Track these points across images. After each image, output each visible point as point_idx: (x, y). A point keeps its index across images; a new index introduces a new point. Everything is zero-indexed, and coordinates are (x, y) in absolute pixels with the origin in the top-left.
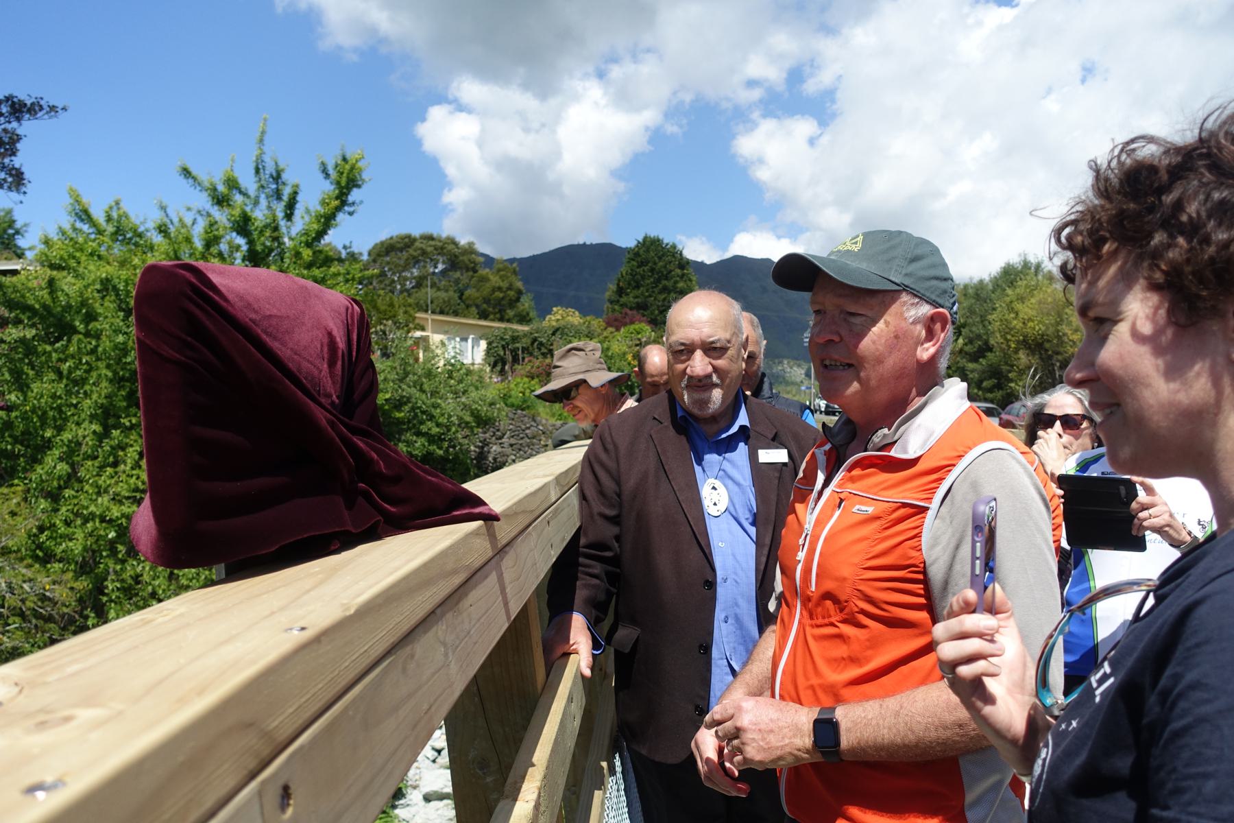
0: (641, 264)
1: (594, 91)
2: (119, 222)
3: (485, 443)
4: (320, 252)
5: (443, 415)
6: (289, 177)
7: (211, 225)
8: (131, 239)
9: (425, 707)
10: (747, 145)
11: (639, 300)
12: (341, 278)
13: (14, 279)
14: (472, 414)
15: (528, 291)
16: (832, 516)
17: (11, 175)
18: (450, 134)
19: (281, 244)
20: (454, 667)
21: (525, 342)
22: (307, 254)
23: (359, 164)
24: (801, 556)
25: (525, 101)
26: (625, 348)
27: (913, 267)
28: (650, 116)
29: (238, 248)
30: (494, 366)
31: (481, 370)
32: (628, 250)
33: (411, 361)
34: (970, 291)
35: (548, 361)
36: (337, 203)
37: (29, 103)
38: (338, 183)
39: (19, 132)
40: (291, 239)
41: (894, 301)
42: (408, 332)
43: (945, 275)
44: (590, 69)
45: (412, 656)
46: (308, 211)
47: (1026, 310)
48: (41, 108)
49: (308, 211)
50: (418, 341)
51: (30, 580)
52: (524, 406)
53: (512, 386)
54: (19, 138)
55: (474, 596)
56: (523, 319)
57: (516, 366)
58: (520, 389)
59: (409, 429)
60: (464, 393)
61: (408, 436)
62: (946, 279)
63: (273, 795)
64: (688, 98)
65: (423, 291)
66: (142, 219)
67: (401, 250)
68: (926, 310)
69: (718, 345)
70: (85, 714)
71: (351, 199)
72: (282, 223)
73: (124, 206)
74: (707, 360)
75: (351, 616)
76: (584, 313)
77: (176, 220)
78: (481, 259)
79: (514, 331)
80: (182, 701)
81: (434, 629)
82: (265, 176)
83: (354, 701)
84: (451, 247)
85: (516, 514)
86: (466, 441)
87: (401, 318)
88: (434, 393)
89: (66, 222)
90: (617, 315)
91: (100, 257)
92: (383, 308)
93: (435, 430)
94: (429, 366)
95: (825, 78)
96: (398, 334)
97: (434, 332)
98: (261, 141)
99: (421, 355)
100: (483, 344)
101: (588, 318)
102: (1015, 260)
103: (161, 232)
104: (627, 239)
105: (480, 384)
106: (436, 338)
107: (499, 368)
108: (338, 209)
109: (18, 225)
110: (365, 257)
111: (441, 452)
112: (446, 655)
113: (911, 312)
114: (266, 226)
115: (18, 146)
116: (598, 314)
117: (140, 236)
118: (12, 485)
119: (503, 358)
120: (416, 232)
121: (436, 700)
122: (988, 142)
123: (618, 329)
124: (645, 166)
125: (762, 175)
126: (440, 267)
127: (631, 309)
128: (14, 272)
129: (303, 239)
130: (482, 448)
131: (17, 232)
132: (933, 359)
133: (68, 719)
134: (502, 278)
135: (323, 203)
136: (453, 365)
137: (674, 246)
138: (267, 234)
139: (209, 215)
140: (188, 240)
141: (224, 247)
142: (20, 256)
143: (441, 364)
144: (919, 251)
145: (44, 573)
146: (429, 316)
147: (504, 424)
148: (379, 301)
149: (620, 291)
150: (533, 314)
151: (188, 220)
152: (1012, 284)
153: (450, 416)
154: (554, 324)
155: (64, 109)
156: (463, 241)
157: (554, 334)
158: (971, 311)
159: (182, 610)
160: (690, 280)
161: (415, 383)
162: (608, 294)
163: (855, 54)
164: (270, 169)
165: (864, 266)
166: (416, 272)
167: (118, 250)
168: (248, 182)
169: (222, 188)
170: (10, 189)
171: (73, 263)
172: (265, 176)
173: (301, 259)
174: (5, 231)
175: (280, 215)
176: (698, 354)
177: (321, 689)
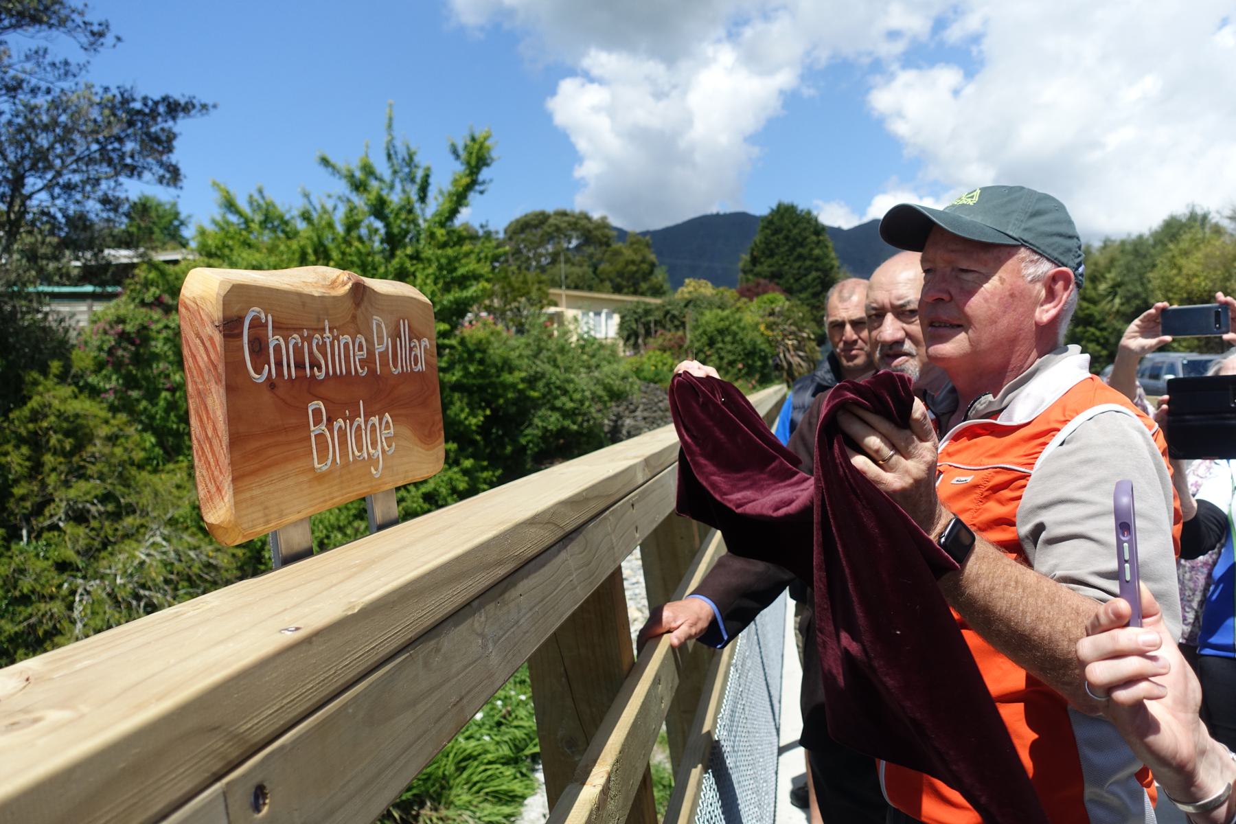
1: (726, 56)
3: (619, 417)
4: (454, 231)
6: (422, 160)
7: (351, 210)
9: (454, 699)
10: (883, 99)
11: (774, 269)
15: (661, 264)
17: (169, 171)
18: (578, 106)
20: (494, 659)
21: (658, 315)
22: (440, 233)
25: (655, 68)
26: (757, 319)
27: (1032, 223)
28: (785, 79)
29: (376, 230)
30: (627, 339)
31: (613, 345)
32: (762, 219)
35: (680, 333)
37: (182, 102)
38: (468, 163)
39: (176, 130)
40: (425, 220)
41: (1010, 256)
42: (542, 308)
43: (1071, 233)
44: (721, 32)
45: (438, 650)
46: (441, 193)
48: (194, 106)
49: (441, 193)
50: (552, 318)
54: (175, 136)
55: (524, 585)
56: (657, 291)
57: (651, 340)
58: (653, 362)
59: (544, 404)
62: (1071, 237)
63: (243, 797)
64: (823, 56)
65: (558, 266)
66: (287, 207)
67: (536, 227)
68: (1046, 268)
69: (909, 308)
70: (54, 716)
71: (481, 177)
72: (417, 206)
73: (270, 195)
74: (899, 324)
75: (353, 615)
76: (716, 282)
77: (318, 207)
78: (615, 233)
79: (646, 304)
81: (470, 621)
83: (355, 699)
84: (584, 222)
86: (600, 415)
87: (534, 295)
90: (751, 284)
92: (517, 285)
93: (570, 405)
95: (972, 23)
96: (532, 310)
97: (569, 307)
98: (390, 126)
100: (616, 319)
101: (721, 289)
102: (1179, 209)
104: (761, 208)
105: (613, 357)
106: (570, 313)
107: (632, 341)
108: (469, 187)
109: (182, 216)
110: (501, 236)
111: (575, 427)
112: (485, 646)
113: (1031, 269)
114: (401, 209)
115: (175, 143)
116: (731, 285)
117: (286, 223)
118: (177, 462)
119: (633, 333)
120: (550, 209)
121: (469, 692)
122: (1150, 84)
123: (751, 300)
125: (901, 128)
126: (574, 243)
127: (765, 278)
129: (437, 219)
130: (616, 421)
131: (182, 223)
132: (1055, 321)
133: (36, 721)
134: (636, 251)
136: (585, 340)
137: (809, 213)
139: (349, 200)
140: (330, 225)
141: (363, 231)
143: (574, 339)
144: (1042, 206)
146: (563, 292)
147: (636, 397)
149: (754, 261)
150: (666, 286)
151: (329, 206)
153: (583, 391)
154: (687, 296)
155: (215, 106)
156: (596, 215)
157: (686, 306)
158: (1129, 269)
159: (216, 603)
160: (827, 247)
161: (549, 358)
162: (741, 265)
164: (402, 152)
165: (979, 219)
166: (550, 248)
167: (267, 237)
168: (382, 168)
169: (359, 175)
170: (168, 184)
171: (227, 251)
174: (171, 222)
175: (414, 197)
176: (889, 318)
177: (311, 689)
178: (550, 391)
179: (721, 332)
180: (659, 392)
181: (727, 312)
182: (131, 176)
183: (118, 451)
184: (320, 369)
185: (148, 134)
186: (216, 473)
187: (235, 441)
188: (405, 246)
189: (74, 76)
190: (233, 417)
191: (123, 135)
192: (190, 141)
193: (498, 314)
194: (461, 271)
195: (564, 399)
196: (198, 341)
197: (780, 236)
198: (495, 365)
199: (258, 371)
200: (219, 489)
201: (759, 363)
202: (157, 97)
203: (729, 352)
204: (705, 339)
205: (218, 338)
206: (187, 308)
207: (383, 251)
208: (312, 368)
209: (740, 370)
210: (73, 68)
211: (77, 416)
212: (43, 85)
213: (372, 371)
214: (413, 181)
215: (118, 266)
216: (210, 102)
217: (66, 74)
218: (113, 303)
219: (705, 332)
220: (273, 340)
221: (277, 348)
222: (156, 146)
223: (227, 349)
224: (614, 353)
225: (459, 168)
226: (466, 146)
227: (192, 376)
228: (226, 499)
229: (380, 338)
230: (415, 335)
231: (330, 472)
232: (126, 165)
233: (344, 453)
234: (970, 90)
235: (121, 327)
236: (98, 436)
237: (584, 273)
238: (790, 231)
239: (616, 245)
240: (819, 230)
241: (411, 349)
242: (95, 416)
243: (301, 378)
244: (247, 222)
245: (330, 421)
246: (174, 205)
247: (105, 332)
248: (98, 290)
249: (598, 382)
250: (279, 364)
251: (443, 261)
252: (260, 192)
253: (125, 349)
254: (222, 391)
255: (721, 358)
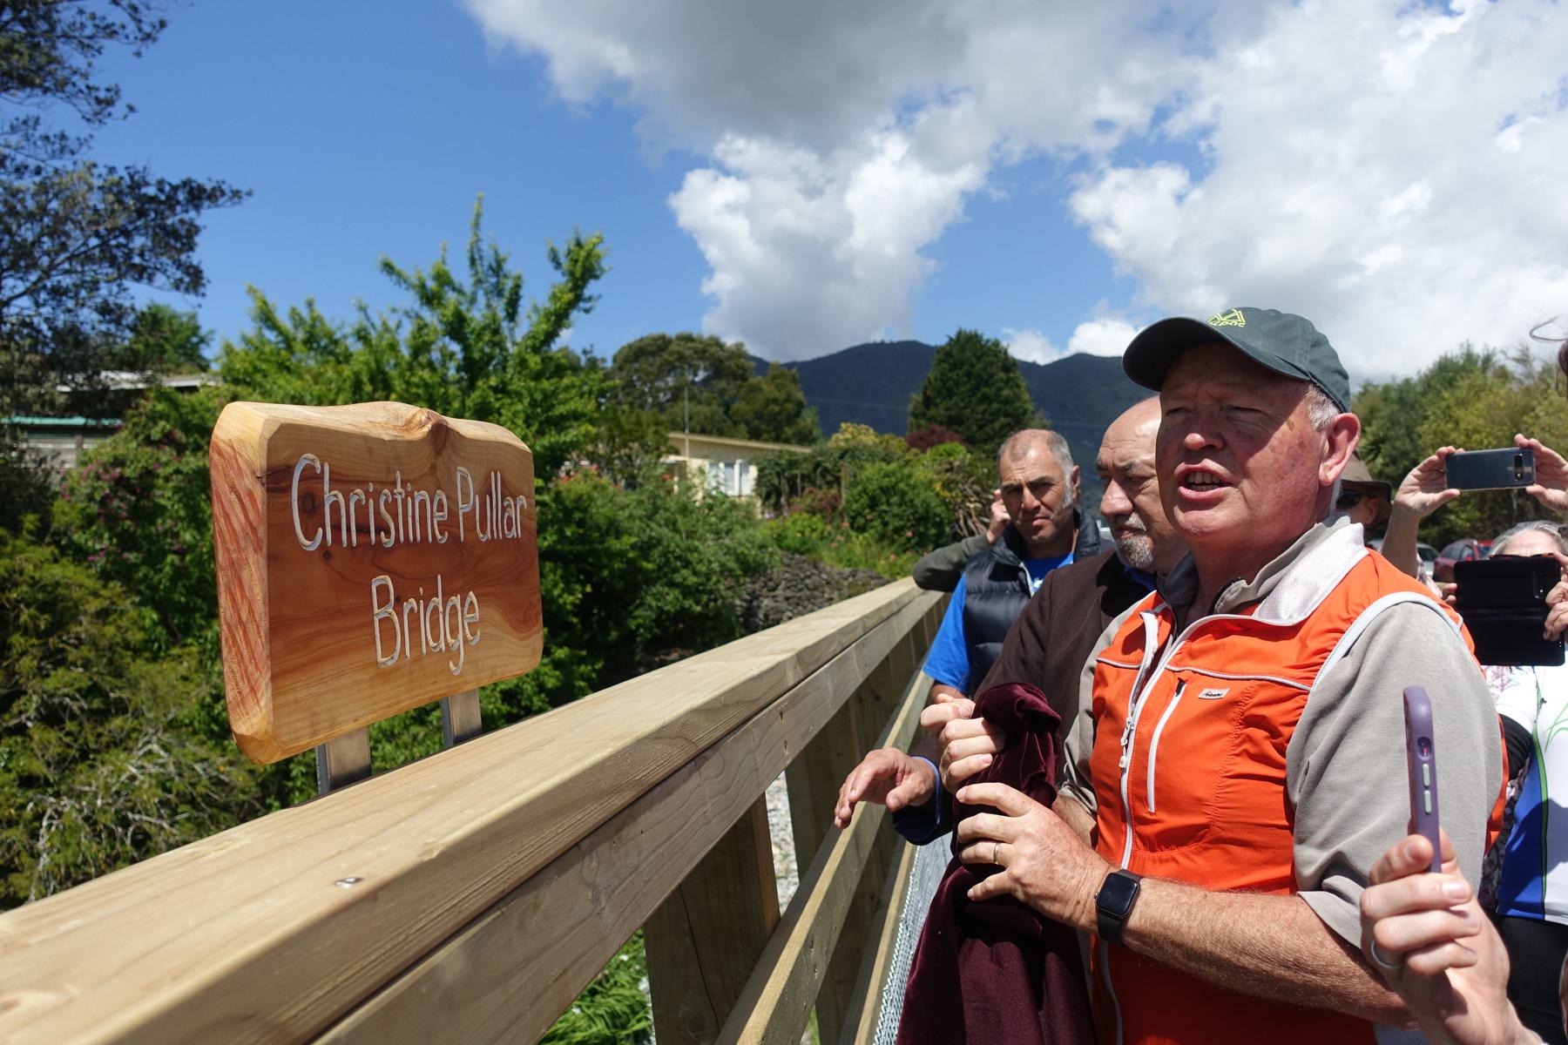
0: (954, 367)
1: (896, 147)
2: (313, 326)
3: (754, 596)
4: (551, 358)
5: (701, 561)
7: (420, 329)
8: (325, 347)
9: (557, 971)
10: (1088, 204)
12: (574, 391)
13: (193, 398)
14: (738, 560)
16: (1167, 704)
17: (188, 274)
18: (709, 204)
19: (504, 349)
21: (806, 468)
23: (598, 250)
24: (1126, 761)
26: (931, 475)
28: (967, 177)
29: (452, 355)
30: (766, 498)
31: (749, 504)
32: (938, 349)
33: (662, 493)
34: (1393, 394)
35: (834, 491)
36: (571, 296)
37: (209, 186)
38: (572, 274)
39: (199, 222)
40: (514, 343)
42: (659, 456)
45: (536, 907)
46: (536, 309)
47: (1471, 418)
48: (223, 194)
49: (536, 309)
51: (203, 760)
52: (803, 549)
53: (788, 523)
55: (646, 820)
56: (804, 438)
57: (796, 500)
58: (799, 527)
60: (728, 532)
61: (658, 588)
66: (338, 322)
67: (653, 354)
71: (587, 293)
72: (505, 324)
73: (319, 309)
75: (431, 862)
76: (880, 429)
77: (378, 324)
79: (794, 454)
80: (149, 989)
81: (577, 867)
82: (482, 268)
84: (714, 349)
85: (726, 706)
86: (730, 593)
87: (650, 440)
88: (691, 534)
89: (251, 329)
90: (924, 431)
91: (288, 369)
92: (628, 427)
93: (693, 580)
94: (684, 498)
95: (1201, 112)
96: (647, 458)
97: (693, 456)
98: (477, 225)
99: (676, 488)
100: (753, 471)
101: (886, 436)
103: (360, 338)
104: (936, 336)
106: (694, 464)
107: (772, 501)
108: (572, 304)
109: (203, 332)
110: (609, 364)
111: (698, 608)
114: (484, 328)
115: (197, 239)
116: (897, 431)
117: (336, 342)
119: (774, 490)
120: (671, 331)
122: (1418, 194)
123: (924, 451)
124: (967, 236)
125: (1111, 240)
126: (701, 375)
127: (941, 424)
128: (192, 389)
129: (529, 343)
130: (750, 602)
131: (202, 340)
134: (779, 387)
135: (554, 297)
136: (712, 497)
137: (997, 344)
138: (486, 338)
139: (418, 316)
140: (393, 347)
141: (435, 355)
142: (204, 368)
143: (700, 496)
145: (218, 751)
146: (687, 437)
147: (777, 572)
148: (623, 418)
149: (928, 402)
150: (817, 432)
151: (392, 324)
152: (1451, 383)
153: (710, 562)
154: (842, 444)
155: (250, 194)
156: (729, 341)
157: (842, 457)
158: (1394, 422)
160: (1018, 386)
161: (667, 520)
162: (911, 407)
163: (1245, 80)
164: (489, 259)
166: (671, 381)
168: (462, 276)
169: (431, 285)
170: (187, 290)
171: (258, 378)
172: (482, 268)
173: (527, 367)
174: (188, 339)
175: (501, 314)
178: (668, 562)
179: (885, 491)
180: (805, 566)
181: (893, 466)
182: (139, 279)
183: (110, 630)
184: (388, 534)
185: (163, 227)
186: (251, 669)
187: (277, 627)
188: (487, 376)
189: (73, 153)
190: (276, 596)
191: (130, 228)
192: (217, 238)
193: (603, 463)
194: (561, 410)
195: (685, 572)
196: (233, 496)
197: (960, 372)
198: (598, 528)
199: (310, 536)
200: (253, 690)
201: (933, 531)
202: (176, 181)
203: (896, 516)
204: (865, 500)
205: (259, 492)
206: (220, 453)
207: (459, 381)
208: (377, 533)
209: (909, 539)
210: (72, 144)
211: (57, 584)
212: (32, 164)
213: (454, 538)
214: (500, 294)
215: (117, 392)
216: (244, 189)
217: (62, 150)
218: (109, 440)
219: (865, 491)
220: (330, 496)
221: (335, 507)
222: (172, 242)
223: (270, 506)
224: (749, 515)
225: (559, 279)
226: (569, 252)
227: (224, 542)
228: (262, 703)
229: (465, 495)
230: (509, 491)
231: (396, 668)
232: (134, 266)
233: (416, 644)
234: (1196, 195)
235: (118, 470)
236: (85, 613)
237: (713, 414)
238: (972, 365)
239: (754, 380)
240: (1010, 365)
241: (504, 509)
242: (81, 586)
243: (364, 545)
244: (288, 342)
245: (399, 601)
246: (193, 317)
247: (98, 478)
248: (92, 422)
249: (729, 551)
250: (336, 527)
251: (538, 396)
252: (310, 304)
253: (122, 499)
254: (263, 562)
255: (885, 524)
